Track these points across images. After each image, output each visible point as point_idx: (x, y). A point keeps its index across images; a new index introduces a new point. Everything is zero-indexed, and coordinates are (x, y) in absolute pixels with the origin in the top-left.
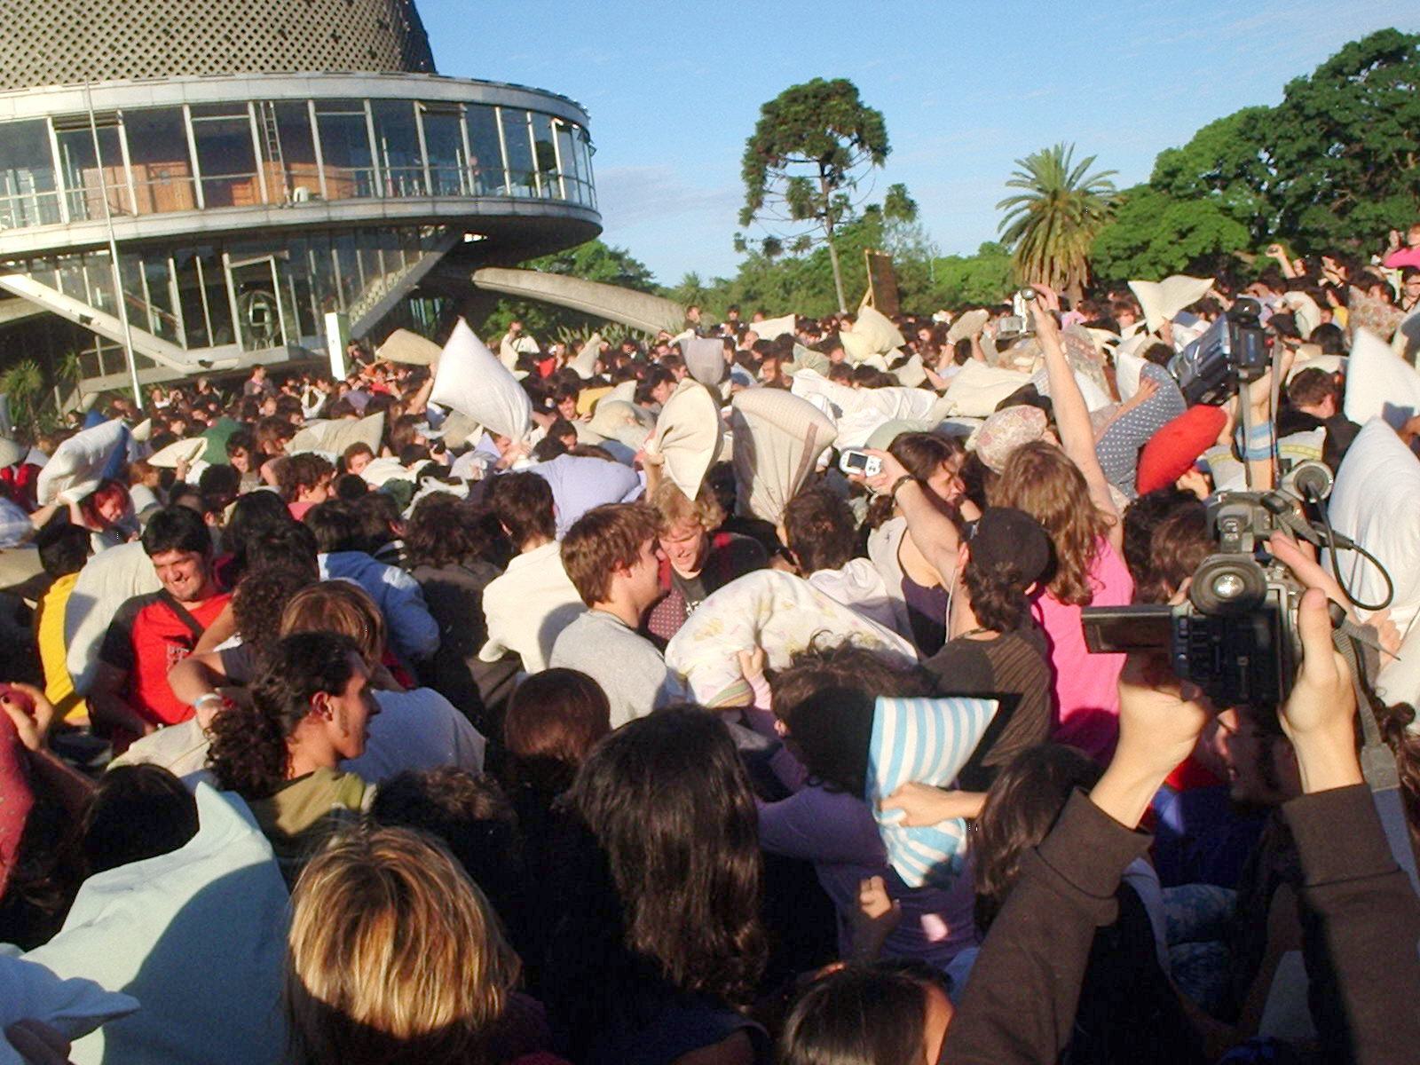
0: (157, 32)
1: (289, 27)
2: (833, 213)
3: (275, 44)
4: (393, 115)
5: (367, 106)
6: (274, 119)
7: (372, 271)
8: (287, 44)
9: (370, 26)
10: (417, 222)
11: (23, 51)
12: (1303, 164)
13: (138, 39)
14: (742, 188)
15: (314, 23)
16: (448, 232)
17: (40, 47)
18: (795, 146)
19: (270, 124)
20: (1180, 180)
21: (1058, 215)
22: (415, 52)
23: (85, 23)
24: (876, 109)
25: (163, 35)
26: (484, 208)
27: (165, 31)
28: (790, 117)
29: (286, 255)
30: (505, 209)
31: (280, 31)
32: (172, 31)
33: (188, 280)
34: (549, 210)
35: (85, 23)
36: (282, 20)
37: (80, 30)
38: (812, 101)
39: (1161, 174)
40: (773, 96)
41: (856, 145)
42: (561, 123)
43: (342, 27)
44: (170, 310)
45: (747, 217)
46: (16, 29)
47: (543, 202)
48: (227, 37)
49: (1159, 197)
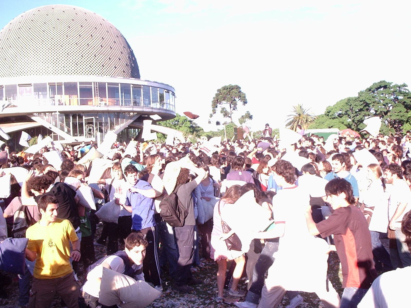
0: (88, 66)
3: (101, 68)
5: (119, 84)
12: (360, 113)
13: (75, 54)
18: (224, 100)
20: (330, 114)
21: (300, 120)
24: (244, 93)
25: (75, 65)
33: (75, 121)
35: (58, 61)
37: (57, 62)
38: (228, 90)
39: (326, 112)
40: (220, 88)
42: (166, 91)
43: (117, 65)
44: (69, 127)
46: (42, 61)
47: (164, 110)
49: (326, 117)
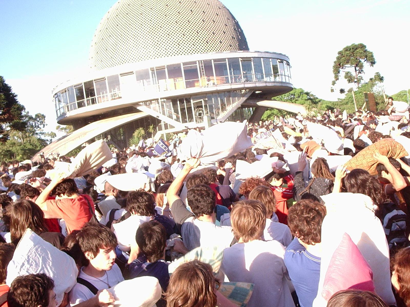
1: (209, 40)
2: (358, 82)
4: (234, 63)
6: (203, 65)
7: (229, 103)
8: (208, 45)
9: (230, 38)
10: (241, 89)
11: (144, 51)
14: (333, 75)
15: (215, 39)
16: (249, 91)
17: (148, 50)
18: (347, 63)
19: (202, 66)
22: (242, 44)
23: (159, 43)
26: (258, 85)
27: (178, 44)
28: (345, 55)
29: (207, 99)
30: (264, 85)
31: (206, 42)
32: (180, 44)
34: (276, 84)
36: (207, 39)
38: (352, 50)
40: (341, 49)
41: (366, 62)
42: (280, 61)
45: (334, 83)
48: (193, 44)
